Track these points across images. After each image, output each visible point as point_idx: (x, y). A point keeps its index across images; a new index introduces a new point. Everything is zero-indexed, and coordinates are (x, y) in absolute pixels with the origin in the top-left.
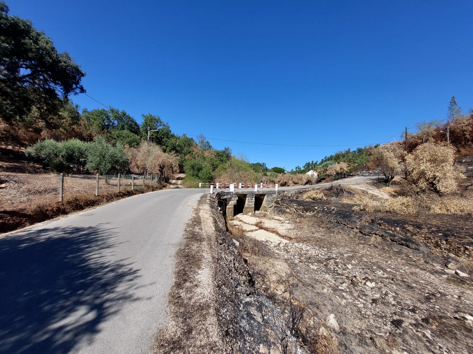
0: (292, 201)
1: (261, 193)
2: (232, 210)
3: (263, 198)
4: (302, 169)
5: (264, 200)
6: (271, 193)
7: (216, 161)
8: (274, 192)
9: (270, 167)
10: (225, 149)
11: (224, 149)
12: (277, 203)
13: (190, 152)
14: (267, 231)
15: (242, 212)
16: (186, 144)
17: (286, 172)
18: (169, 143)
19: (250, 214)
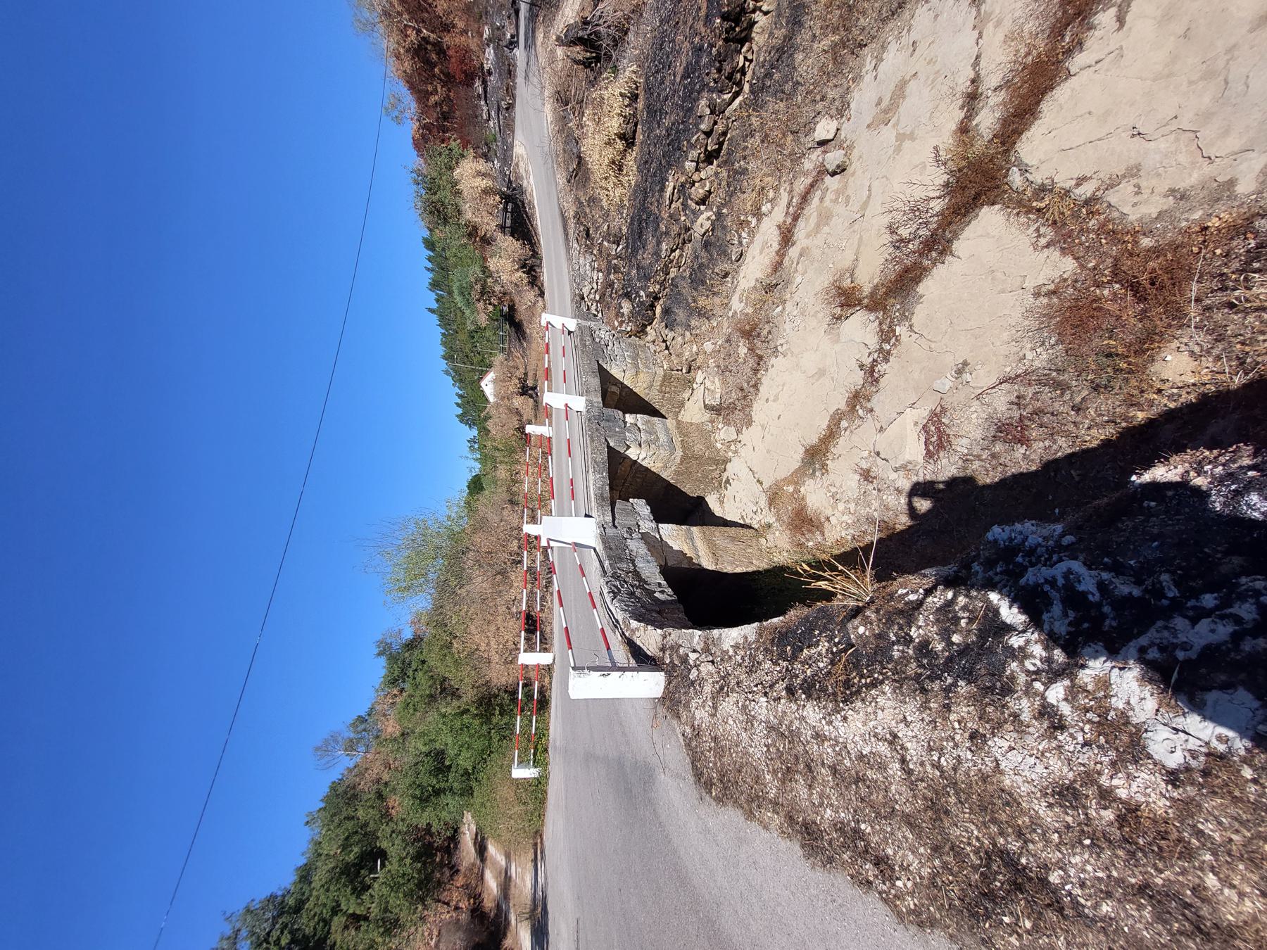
10: (380, 654)
11: (383, 661)
13: (380, 796)
16: (344, 814)
18: (323, 899)
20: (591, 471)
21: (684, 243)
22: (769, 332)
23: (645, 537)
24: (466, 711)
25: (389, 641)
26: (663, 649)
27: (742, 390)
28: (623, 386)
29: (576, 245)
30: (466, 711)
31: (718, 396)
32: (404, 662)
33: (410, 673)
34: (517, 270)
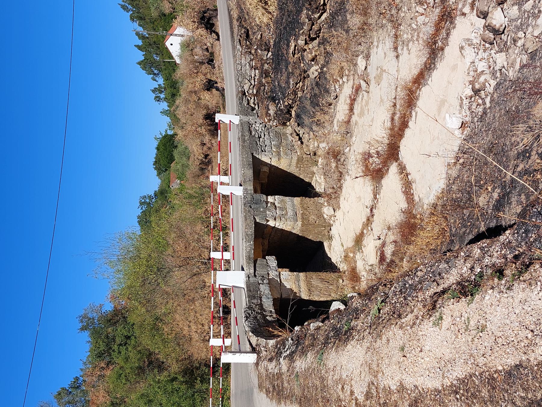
0: (279, 60)
1: (250, 173)
2: (315, 278)
3: (265, 169)
4: (161, 81)
5: (274, 163)
6: (250, 140)
7: (127, 359)
8: (246, 128)
9: (152, 183)
10: (83, 329)
11: (86, 335)
12: (284, 117)
14: (404, 125)
15: (320, 245)
17: (170, 133)
19: (327, 211)
20: (245, 240)
21: (305, 78)
22: (344, 161)
23: (271, 283)
24: (174, 379)
25: (90, 315)
26: (257, 345)
27: (333, 188)
28: (271, 166)
29: (239, 47)
30: (174, 379)
31: (323, 187)
32: (107, 337)
33: (116, 347)
34: (197, 28)
